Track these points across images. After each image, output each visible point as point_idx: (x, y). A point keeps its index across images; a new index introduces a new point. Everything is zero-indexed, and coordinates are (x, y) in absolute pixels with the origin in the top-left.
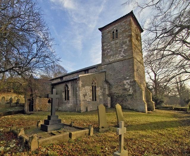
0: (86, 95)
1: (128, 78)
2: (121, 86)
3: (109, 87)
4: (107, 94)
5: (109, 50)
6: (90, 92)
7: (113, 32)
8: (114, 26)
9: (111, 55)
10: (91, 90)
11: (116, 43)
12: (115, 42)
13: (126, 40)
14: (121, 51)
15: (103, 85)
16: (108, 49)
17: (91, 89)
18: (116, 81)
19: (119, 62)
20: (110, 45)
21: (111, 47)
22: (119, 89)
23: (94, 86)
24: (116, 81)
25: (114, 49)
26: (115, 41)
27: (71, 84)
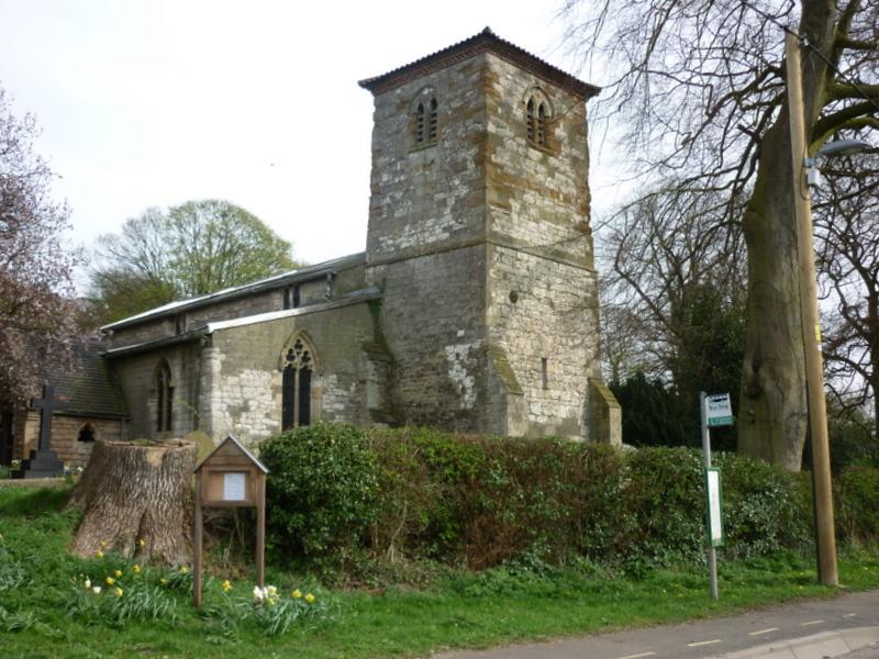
0: (245, 408)
1: (461, 333)
2: (434, 369)
3: (390, 376)
4: (372, 410)
5: (399, 195)
6: (268, 397)
7: (421, 108)
8: (422, 81)
9: (403, 221)
10: (274, 388)
11: (427, 165)
12: (425, 158)
13: (463, 155)
14: (443, 203)
15: (355, 364)
16: (397, 186)
17: (279, 380)
18: (418, 346)
19: (433, 257)
20: (402, 171)
21: (409, 181)
22: (426, 384)
23: (299, 367)
24: (418, 346)
25: (420, 192)
26: (422, 153)
27: (183, 359)
